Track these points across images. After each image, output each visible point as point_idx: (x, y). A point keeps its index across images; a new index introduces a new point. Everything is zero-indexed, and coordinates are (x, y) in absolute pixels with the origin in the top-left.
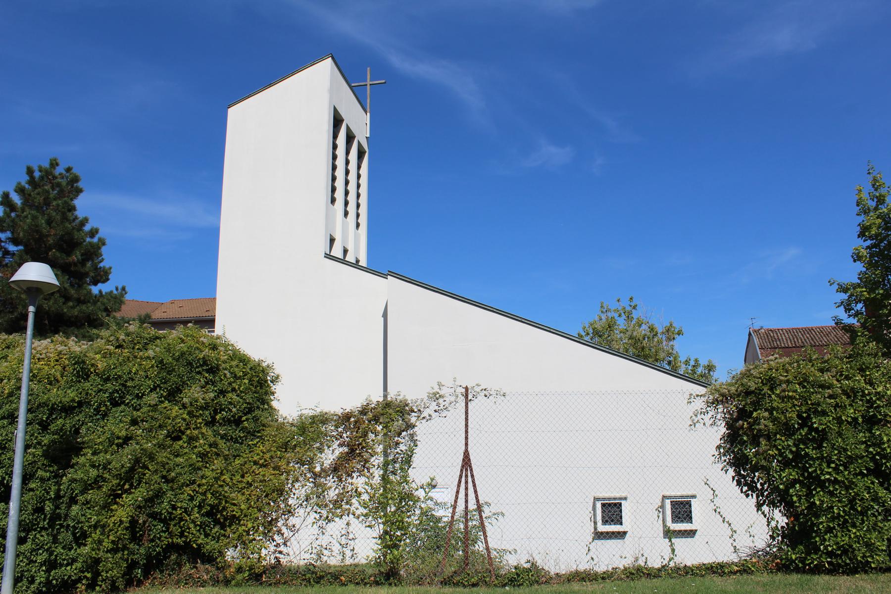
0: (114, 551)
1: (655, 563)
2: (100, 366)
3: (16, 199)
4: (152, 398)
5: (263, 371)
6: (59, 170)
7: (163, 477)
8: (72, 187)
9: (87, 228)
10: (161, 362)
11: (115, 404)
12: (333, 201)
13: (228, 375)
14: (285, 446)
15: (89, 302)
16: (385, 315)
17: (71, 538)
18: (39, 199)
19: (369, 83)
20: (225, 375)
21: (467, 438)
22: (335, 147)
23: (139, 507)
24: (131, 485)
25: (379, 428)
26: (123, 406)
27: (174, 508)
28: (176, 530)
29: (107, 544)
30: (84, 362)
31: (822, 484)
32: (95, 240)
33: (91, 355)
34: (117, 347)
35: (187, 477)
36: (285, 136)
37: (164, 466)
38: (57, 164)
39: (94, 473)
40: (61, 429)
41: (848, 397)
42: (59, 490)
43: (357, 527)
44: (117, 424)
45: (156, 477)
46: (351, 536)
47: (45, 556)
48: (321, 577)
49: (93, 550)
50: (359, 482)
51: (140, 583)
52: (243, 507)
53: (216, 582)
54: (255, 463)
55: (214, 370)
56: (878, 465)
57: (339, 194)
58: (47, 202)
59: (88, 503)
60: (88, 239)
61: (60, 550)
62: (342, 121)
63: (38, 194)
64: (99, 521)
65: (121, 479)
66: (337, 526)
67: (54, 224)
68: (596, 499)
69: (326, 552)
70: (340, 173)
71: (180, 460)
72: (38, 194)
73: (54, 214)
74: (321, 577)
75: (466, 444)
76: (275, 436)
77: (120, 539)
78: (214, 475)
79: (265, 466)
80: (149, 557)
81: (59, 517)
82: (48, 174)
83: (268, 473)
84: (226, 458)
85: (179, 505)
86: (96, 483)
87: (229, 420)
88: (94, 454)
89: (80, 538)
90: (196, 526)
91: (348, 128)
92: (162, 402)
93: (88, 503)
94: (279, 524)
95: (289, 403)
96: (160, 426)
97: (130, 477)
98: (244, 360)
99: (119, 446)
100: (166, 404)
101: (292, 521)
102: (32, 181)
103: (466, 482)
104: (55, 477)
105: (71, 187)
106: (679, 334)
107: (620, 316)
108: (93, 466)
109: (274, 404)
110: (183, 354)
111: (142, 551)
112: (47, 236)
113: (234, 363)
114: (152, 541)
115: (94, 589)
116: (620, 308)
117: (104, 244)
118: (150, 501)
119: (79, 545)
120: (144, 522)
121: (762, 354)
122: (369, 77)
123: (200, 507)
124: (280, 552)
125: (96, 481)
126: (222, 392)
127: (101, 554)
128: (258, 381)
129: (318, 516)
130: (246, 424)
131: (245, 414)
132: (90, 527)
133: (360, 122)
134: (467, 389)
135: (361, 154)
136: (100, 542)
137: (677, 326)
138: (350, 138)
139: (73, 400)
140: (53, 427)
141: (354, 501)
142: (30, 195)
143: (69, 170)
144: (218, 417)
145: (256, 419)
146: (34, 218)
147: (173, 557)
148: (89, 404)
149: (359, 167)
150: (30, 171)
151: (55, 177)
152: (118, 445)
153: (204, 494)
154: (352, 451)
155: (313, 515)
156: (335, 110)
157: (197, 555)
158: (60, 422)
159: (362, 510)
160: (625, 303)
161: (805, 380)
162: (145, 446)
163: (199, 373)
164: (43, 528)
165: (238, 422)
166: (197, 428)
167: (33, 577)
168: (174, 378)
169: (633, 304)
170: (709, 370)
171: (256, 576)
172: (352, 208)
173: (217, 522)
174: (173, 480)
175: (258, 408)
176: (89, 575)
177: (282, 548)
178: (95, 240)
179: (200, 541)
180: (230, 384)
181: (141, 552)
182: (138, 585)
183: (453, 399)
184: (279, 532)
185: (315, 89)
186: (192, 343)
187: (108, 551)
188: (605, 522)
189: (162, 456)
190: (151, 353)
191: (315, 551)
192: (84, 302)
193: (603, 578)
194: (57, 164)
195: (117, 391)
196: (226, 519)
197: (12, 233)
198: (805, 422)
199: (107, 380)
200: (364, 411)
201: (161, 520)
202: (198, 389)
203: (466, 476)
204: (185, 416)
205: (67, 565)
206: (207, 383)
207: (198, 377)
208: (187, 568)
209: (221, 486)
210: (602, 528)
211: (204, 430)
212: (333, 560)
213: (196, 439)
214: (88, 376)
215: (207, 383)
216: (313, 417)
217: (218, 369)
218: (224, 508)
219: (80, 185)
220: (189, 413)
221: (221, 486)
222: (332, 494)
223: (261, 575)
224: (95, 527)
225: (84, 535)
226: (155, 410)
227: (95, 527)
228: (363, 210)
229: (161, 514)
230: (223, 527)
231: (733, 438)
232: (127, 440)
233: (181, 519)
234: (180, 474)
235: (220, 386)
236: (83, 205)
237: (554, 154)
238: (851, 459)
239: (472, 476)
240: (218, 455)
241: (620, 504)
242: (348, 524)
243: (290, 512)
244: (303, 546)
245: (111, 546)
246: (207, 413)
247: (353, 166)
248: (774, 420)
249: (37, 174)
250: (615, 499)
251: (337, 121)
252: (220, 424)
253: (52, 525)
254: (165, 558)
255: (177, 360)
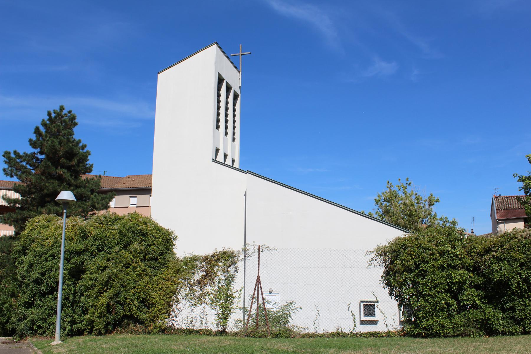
0: (100, 317)
1: (347, 331)
2: (92, 232)
3: (42, 130)
4: (117, 248)
5: (169, 235)
6: (65, 112)
7: (121, 285)
8: (72, 122)
9: (81, 145)
10: (120, 231)
11: (100, 251)
12: (218, 127)
13: (152, 237)
14: (178, 271)
15: (82, 186)
16: (245, 195)
17: (81, 311)
18: (54, 130)
19: (241, 54)
20: (150, 237)
21: (259, 270)
22: (219, 95)
23: (111, 298)
24: (107, 288)
25: (220, 264)
26: (103, 252)
27: (126, 299)
28: (127, 309)
29: (97, 314)
30: (85, 231)
31: (423, 296)
32: (85, 151)
33: (88, 227)
34: (100, 224)
35: (132, 285)
36: (190, 89)
37: (122, 280)
38: (64, 109)
39: (91, 282)
40: (76, 262)
41: (440, 255)
42: (75, 290)
43: (208, 309)
44: (100, 260)
45: (118, 285)
46: (205, 313)
47: (70, 319)
48: (191, 332)
49: (91, 316)
50: (209, 288)
51: (111, 332)
52: (157, 299)
53: (145, 332)
54: (164, 279)
55: (145, 235)
56: (450, 287)
57: (222, 123)
58: (59, 131)
59: (88, 296)
60: (81, 151)
61: (76, 316)
62: (224, 80)
63: (54, 127)
64: (93, 304)
65: (103, 285)
66: (199, 308)
67: (63, 144)
68: (361, 302)
69: (194, 320)
70: (222, 111)
71: (129, 277)
72: (54, 127)
73: (63, 138)
74: (191, 332)
75: (259, 272)
76: (174, 266)
77: (102, 312)
78: (144, 284)
79: (168, 281)
80: (115, 320)
81: (75, 302)
82: (59, 115)
83: (169, 283)
84: (150, 276)
85: (128, 297)
86: (92, 287)
87: (152, 258)
88: (91, 274)
89: (85, 312)
90: (136, 307)
91: (227, 83)
92: (121, 250)
93: (88, 296)
94: (174, 307)
95: (182, 250)
96: (120, 262)
97: (107, 285)
98: (160, 229)
99: (102, 270)
100: (123, 251)
101: (179, 306)
102: (50, 119)
103: (258, 290)
104: (73, 284)
105: (72, 122)
106: (437, 202)
107: (400, 189)
108: (91, 279)
109: (174, 250)
110: (130, 227)
111: (112, 318)
112: (59, 151)
113: (155, 231)
114: (116, 313)
115: (91, 334)
116: (400, 185)
117: (90, 154)
118: (116, 295)
119: (85, 314)
120: (113, 305)
121: (497, 213)
122: (241, 50)
123: (138, 299)
124: (174, 320)
125: (92, 286)
126: (149, 245)
127: (94, 318)
128: (167, 240)
129: (191, 304)
130: (160, 260)
131: (160, 256)
132: (89, 306)
133: (235, 79)
134: (259, 246)
135: (236, 97)
136: (94, 313)
137: (436, 197)
138: (229, 89)
139: (81, 249)
140: (72, 261)
141: (207, 297)
142: (49, 127)
143: (70, 112)
144: (147, 257)
145: (165, 258)
146: (53, 141)
147: (126, 321)
148: (88, 251)
149: (235, 105)
150: (49, 114)
151: (62, 117)
152: (101, 270)
153: (140, 293)
154: (207, 274)
155: (188, 303)
156: (219, 74)
157: (137, 321)
158: (75, 259)
159: (210, 302)
160: (404, 182)
161: (420, 246)
162: (113, 271)
163: (138, 236)
164: (69, 307)
165: (156, 259)
166: (137, 262)
167: (65, 328)
168: (126, 239)
169: (408, 182)
170: (454, 225)
171: (163, 330)
172: (230, 130)
173: (145, 306)
174: (126, 286)
175: (166, 252)
176: (89, 327)
177: (174, 318)
178: (85, 151)
179: (138, 314)
180: (153, 241)
181: (111, 318)
182: (110, 333)
183: (253, 251)
184: (173, 311)
185: (207, 62)
186: (135, 222)
187: (97, 317)
188: (365, 315)
189: (121, 275)
190: (116, 227)
191: (189, 320)
192: (79, 187)
193: (320, 337)
194: (64, 109)
195: (100, 245)
196: (149, 304)
197: (41, 149)
198: (417, 267)
199: (96, 239)
200: (213, 256)
201: (120, 304)
202: (137, 244)
203: (258, 287)
204: (131, 257)
205: (80, 323)
206: (142, 241)
207: (138, 238)
208: (132, 326)
209: (147, 289)
210: (364, 318)
211: (140, 264)
212: (197, 326)
213: (136, 268)
214: (87, 238)
215: (142, 241)
216: (191, 258)
217: (147, 234)
218: (149, 300)
219: (76, 121)
220: (133, 256)
221: (147, 289)
222: (197, 294)
223: (165, 330)
224: (92, 306)
225: (87, 310)
226: (118, 254)
227: (92, 306)
228: (237, 130)
229: (120, 301)
230: (148, 308)
231: (387, 273)
232: (105, 268)
233: (129, 304)
234: (129, 283)
235: (148, 242)
236: (78, 134)
237: (384, 68)
238: (436, 286)
239: (261, 287)
240: (146, 275)
241: (374, 305)
242: (204, 308)
243: (178, 302)
244: (184, 318)
245: (98, 315)
246: (142, 255)
247: (231, 106)
248: (403, 265)
249: (53, 115)
250: (371, 302)
251: (220, 80)
252: (148, 260)
253: (72, 305)
254: (122, 321)
255: (128, 230)
